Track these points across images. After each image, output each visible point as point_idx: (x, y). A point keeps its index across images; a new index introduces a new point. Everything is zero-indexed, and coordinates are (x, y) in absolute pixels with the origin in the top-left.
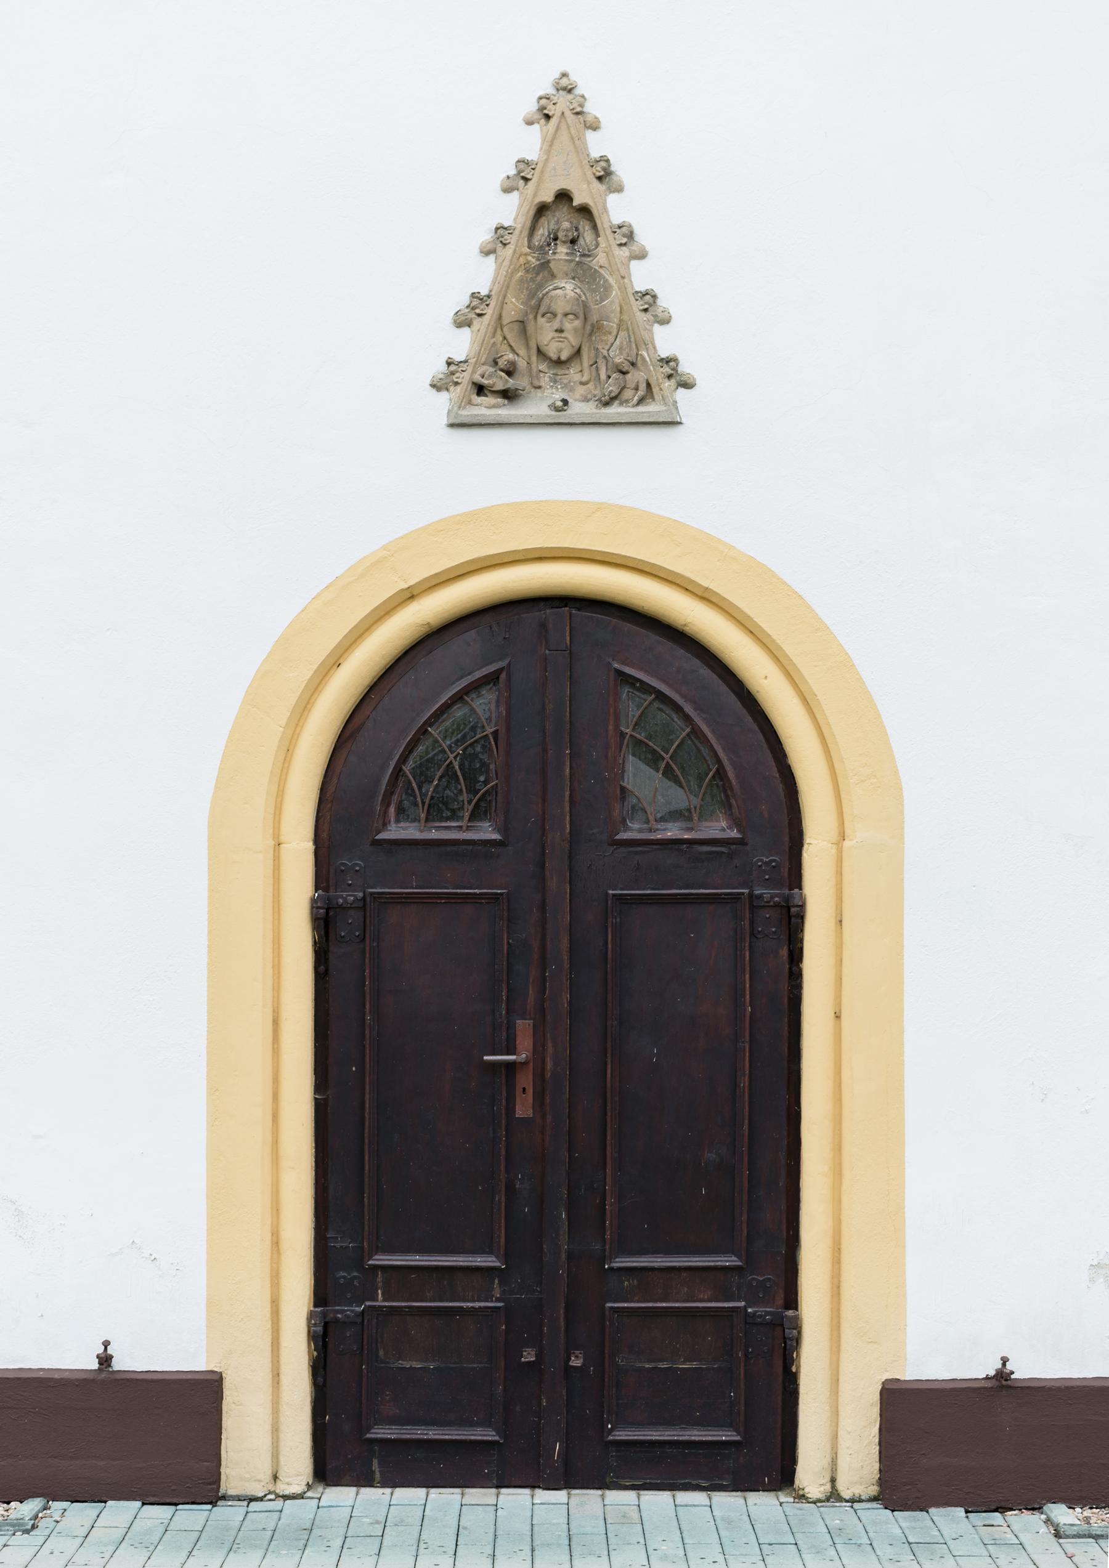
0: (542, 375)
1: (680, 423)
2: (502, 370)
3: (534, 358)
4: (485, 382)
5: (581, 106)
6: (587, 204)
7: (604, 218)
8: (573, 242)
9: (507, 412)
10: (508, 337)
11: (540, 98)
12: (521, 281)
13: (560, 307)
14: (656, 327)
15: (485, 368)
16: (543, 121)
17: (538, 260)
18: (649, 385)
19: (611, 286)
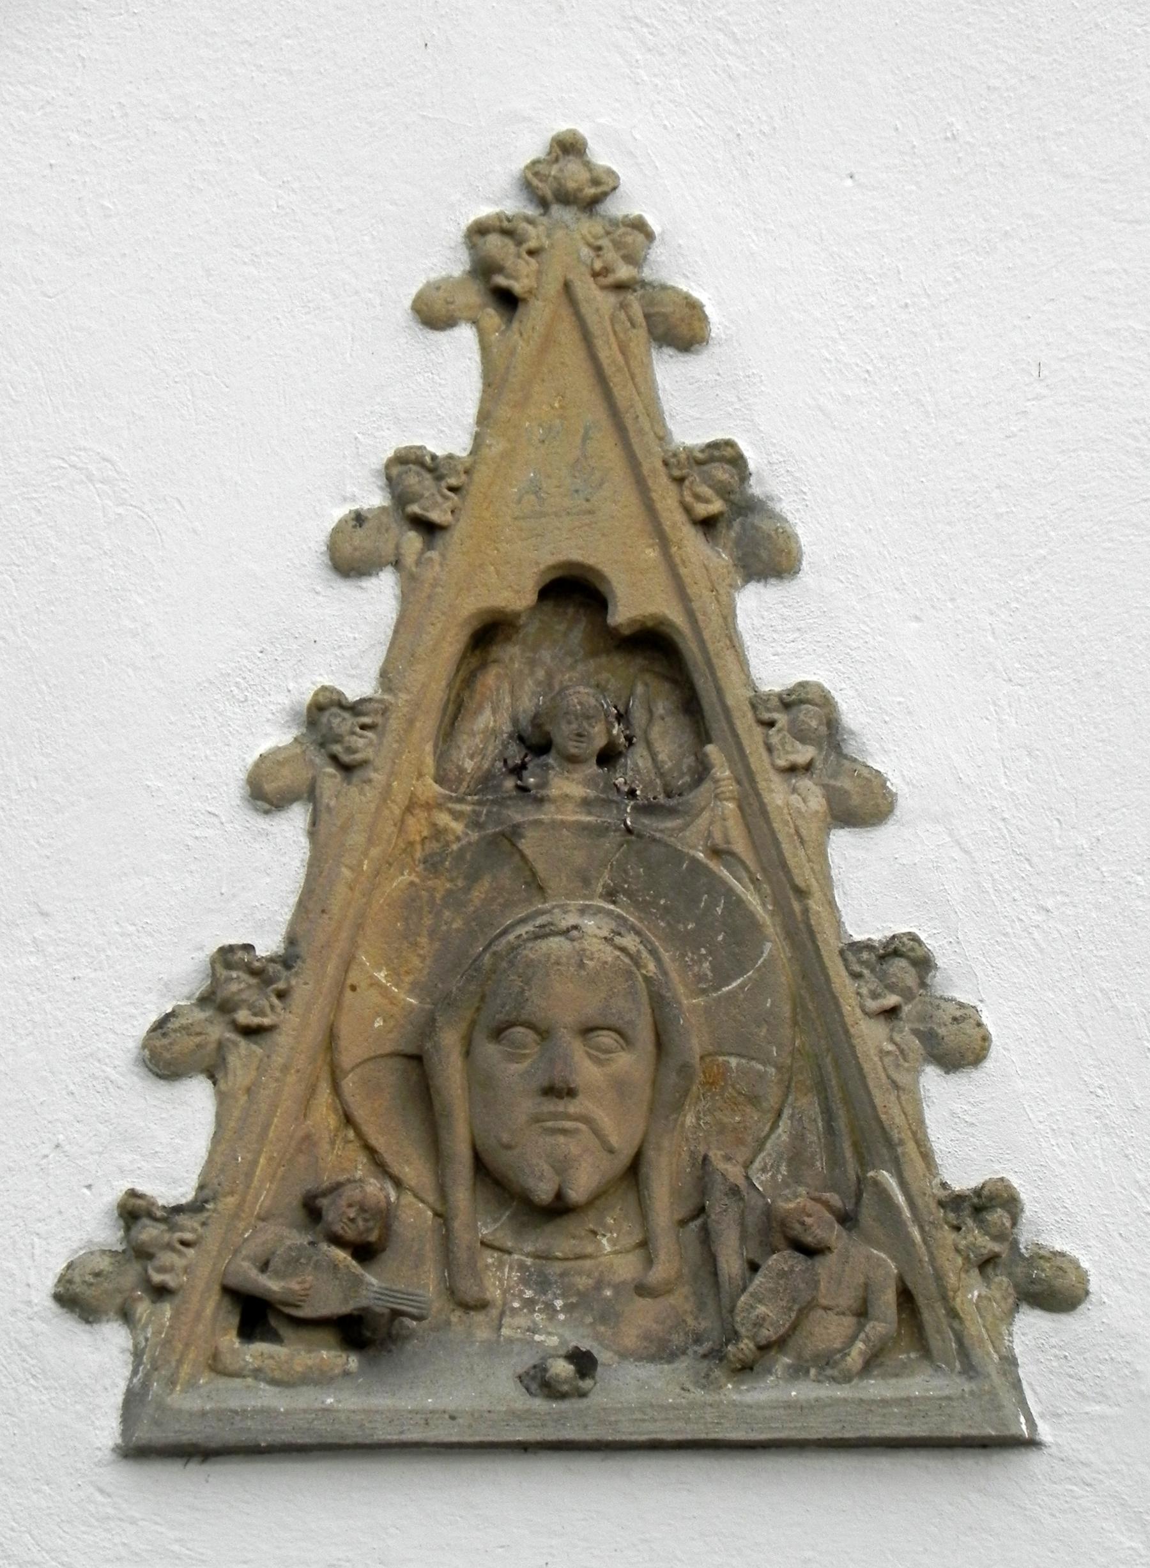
0: (490, 1258)
1: (1032, 1443)
2: (336, 1240)
3: (462, 1195)
4: (272, 1285)
5: (633, 259)
6: (663, 621)
7: (726, 665)
8: (608, 757)
9: (348, 1396)
10: (360, 1114)
11: (479, 230)
12: (409, 903)
13: (564, 1001)
14: (931, 1080)
15: (271, 1232)
16: (492, 317)
17: (475, 824)
18: (906, 1297)
19: (754, 925)
